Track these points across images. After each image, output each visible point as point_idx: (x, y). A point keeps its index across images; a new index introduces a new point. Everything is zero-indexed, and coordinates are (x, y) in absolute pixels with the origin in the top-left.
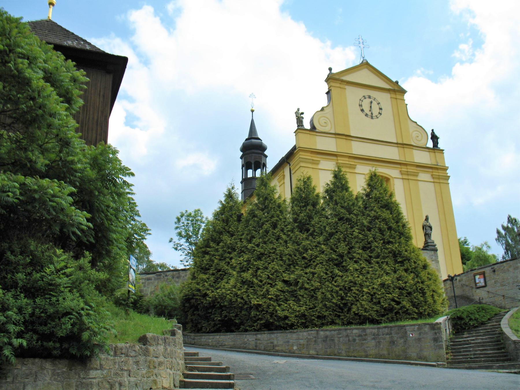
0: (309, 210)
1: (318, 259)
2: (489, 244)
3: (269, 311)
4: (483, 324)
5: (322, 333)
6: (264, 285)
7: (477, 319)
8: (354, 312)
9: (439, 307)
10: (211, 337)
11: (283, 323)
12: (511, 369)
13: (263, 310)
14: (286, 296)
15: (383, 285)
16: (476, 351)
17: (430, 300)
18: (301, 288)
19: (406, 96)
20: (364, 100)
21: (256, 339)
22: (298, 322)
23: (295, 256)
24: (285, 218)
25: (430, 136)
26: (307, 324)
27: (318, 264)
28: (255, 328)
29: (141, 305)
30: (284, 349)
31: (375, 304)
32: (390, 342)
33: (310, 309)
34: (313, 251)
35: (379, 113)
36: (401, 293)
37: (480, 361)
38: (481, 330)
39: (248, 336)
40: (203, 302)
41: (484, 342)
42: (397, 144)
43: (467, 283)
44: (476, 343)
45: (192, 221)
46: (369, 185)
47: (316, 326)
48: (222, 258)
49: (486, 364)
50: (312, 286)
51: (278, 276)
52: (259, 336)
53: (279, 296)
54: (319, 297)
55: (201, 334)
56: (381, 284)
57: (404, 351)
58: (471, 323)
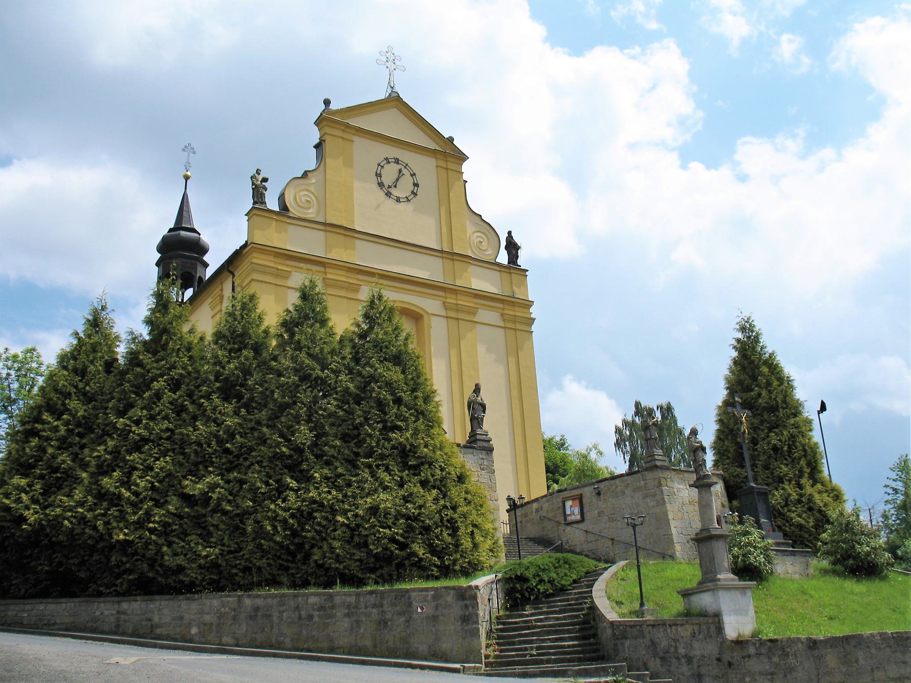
0: (247, 359)
1: (253, 454)
2: (601, 448)
3: (147, 556)
4: (563, 590)
5: (248, 602)
6: (141, 502)
7: (554, 580)
8: (316, 561)
9: (483, 555)
10: (28, 607)
11: (175, 581)
12: (599, 676)
13: (133, 555)
14: (185, 526)
15: (374, 510)
16: (544, 641)
17: (466, 543)
18: (215, 511)
19: (466, 167)
20: (386, 166)
21: (118, 612)
22: (203, 580)
23: (209, 445)
24: (198, 372)
25: (503, 243)
26: (223, 582)
27: (252, 464)
28: (118, 589)
30: (172, 633)
31: (358, 546)
32: (380, 622)
33: (230, 552)
34: (246, 438)
35: (413, 192)
36: (409, 526)
37: (548, 661)
38: (559, 602)
39: (102, 605)
40: (14, 534)
41: (560, 625)
42: (442, 251)
43: (550, 515)
44: (545, 626)
45: (19, 370)
46: (366, 316)
47: (240, 587)
48: (64, 444)
49: (556, 667)
50: (237, 506)
51: (173, 486)
52: (125, 606)
53: (170, 525)
54: (249, 529)
55: (9, 601)
56: (371, 508)
57: (405, 640)
58: (541, 588)
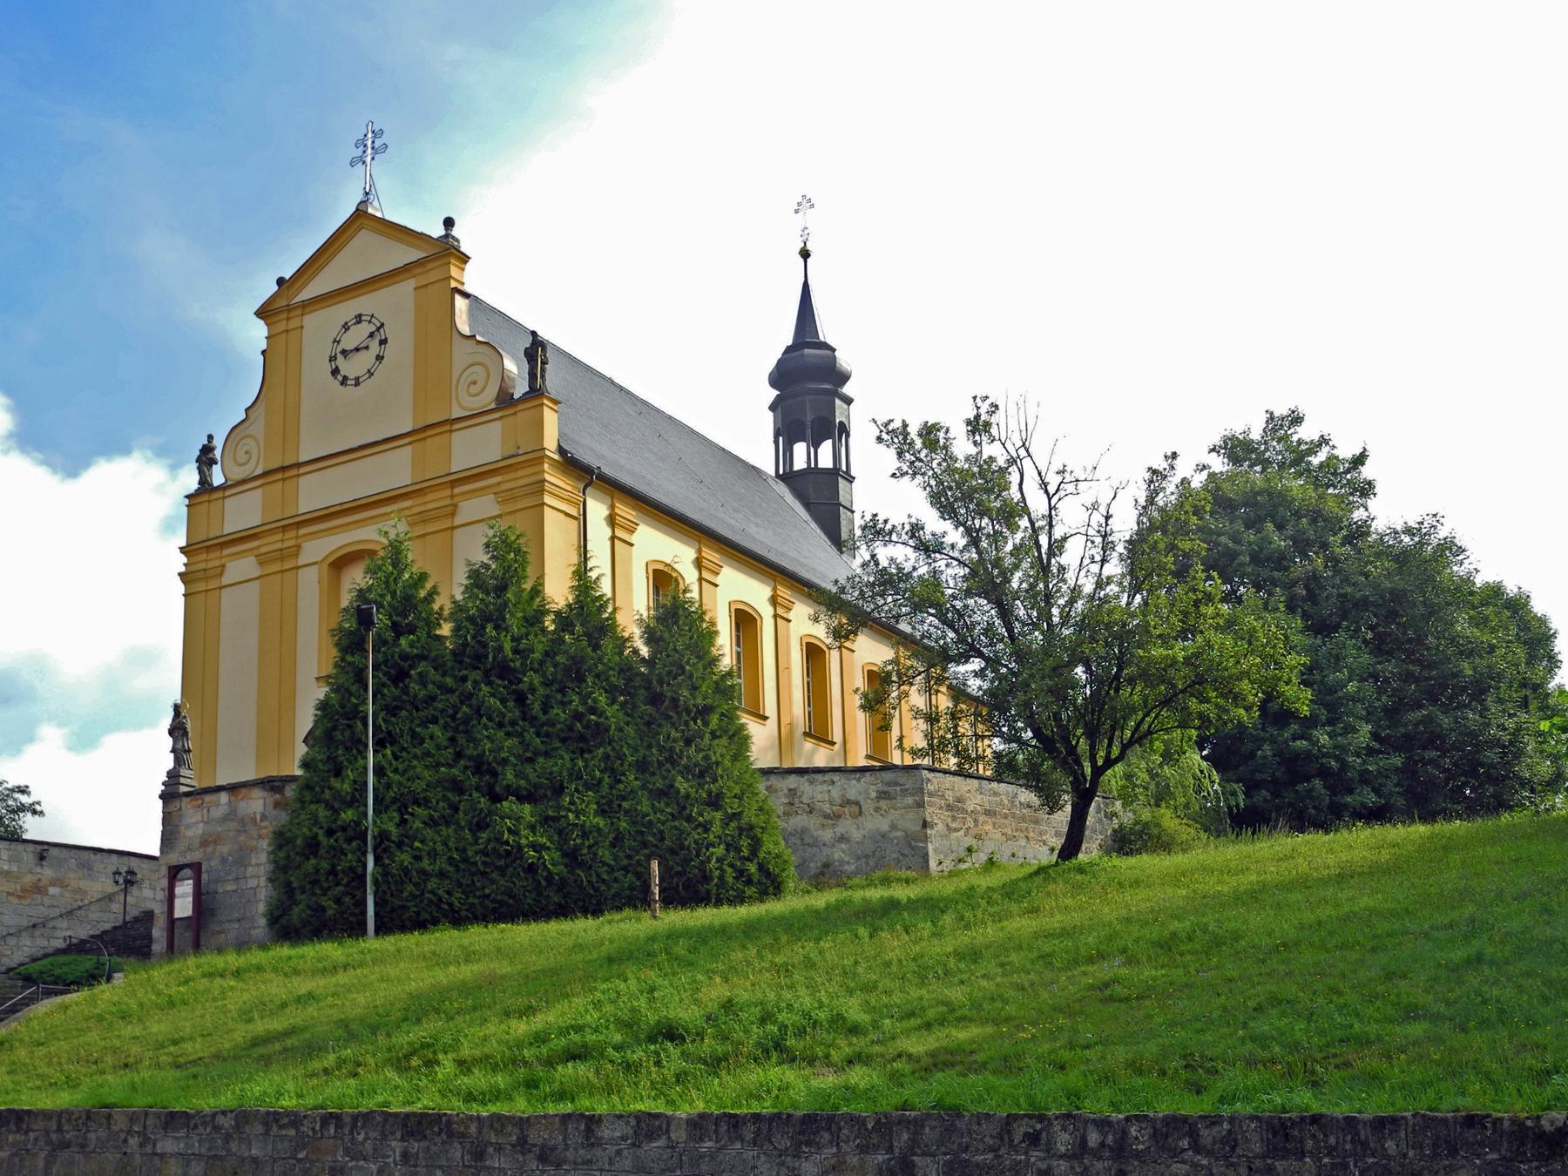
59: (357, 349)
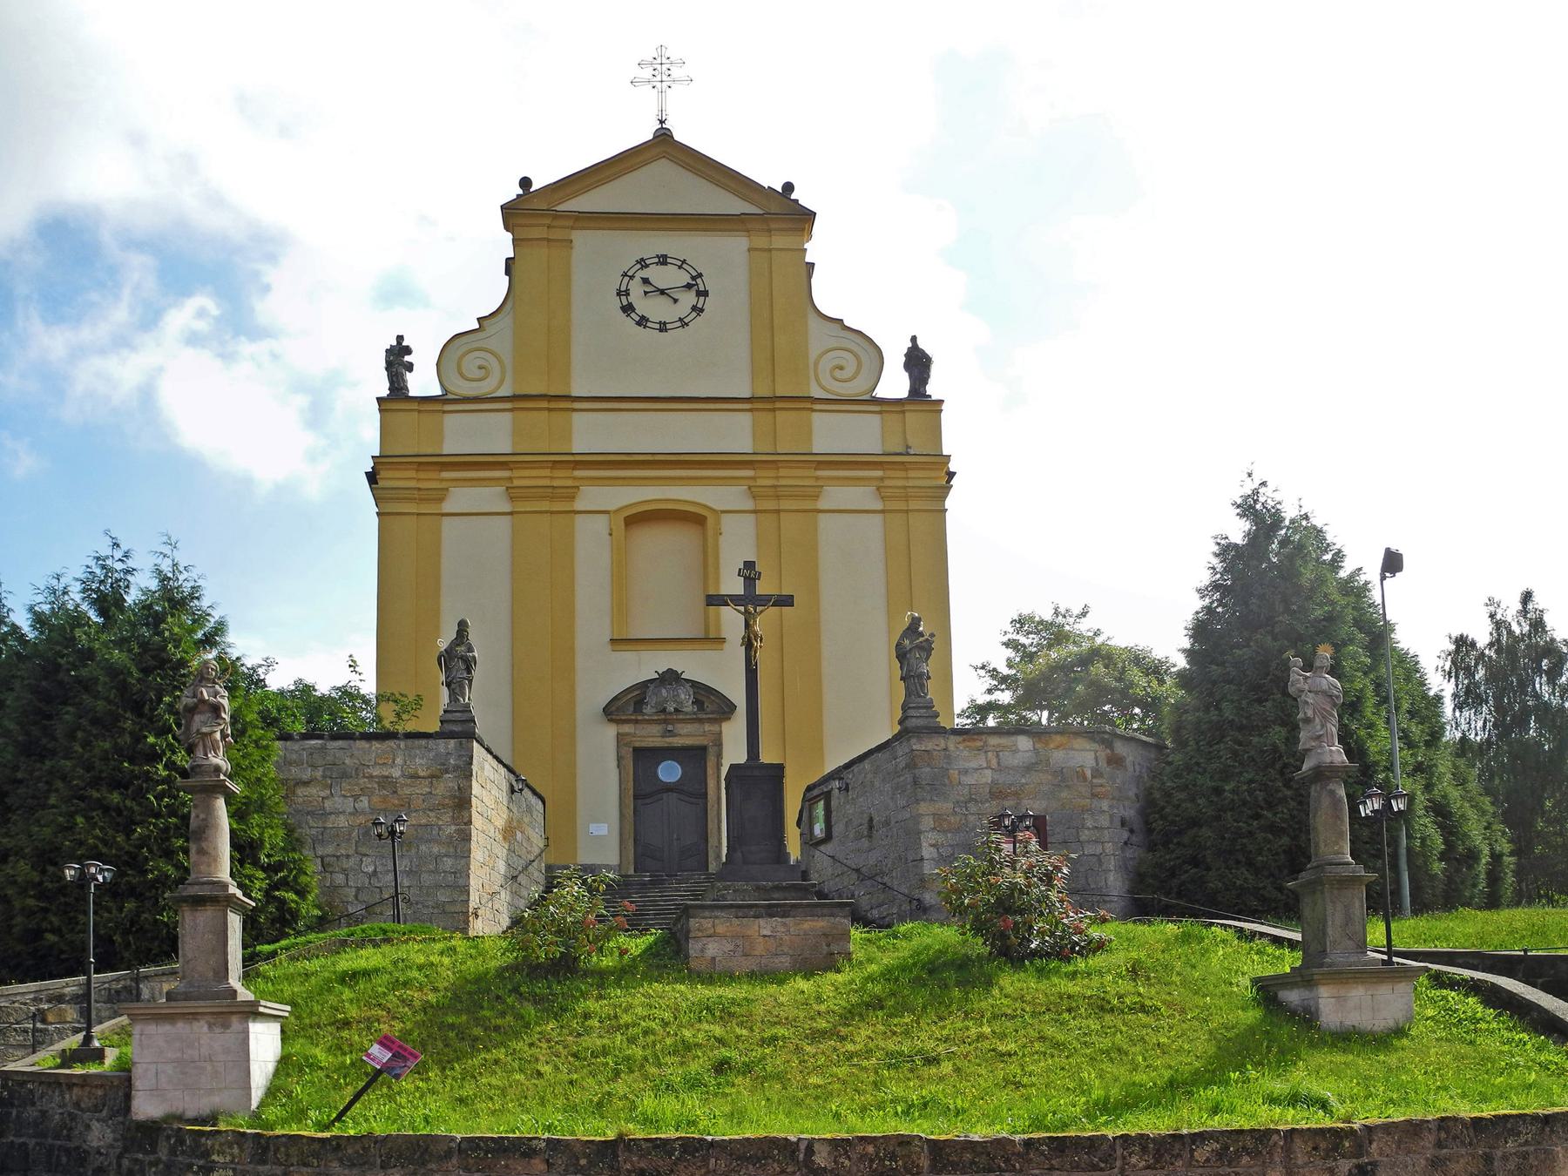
29: (1207, 709)
59: (662, 292)
